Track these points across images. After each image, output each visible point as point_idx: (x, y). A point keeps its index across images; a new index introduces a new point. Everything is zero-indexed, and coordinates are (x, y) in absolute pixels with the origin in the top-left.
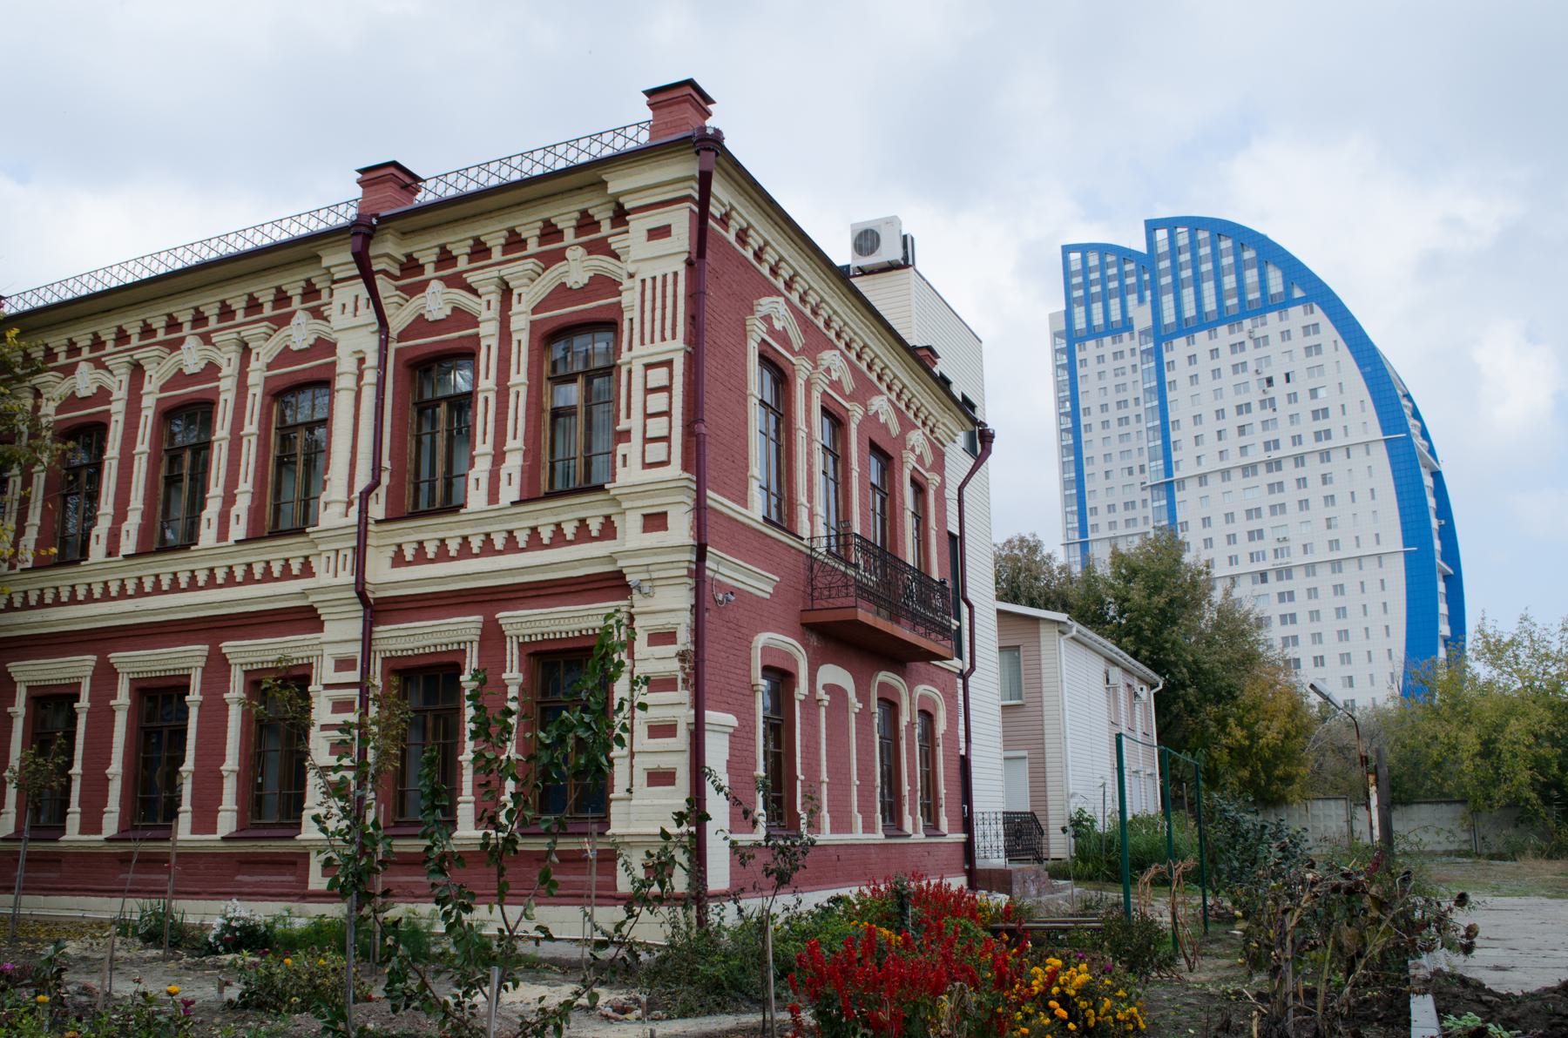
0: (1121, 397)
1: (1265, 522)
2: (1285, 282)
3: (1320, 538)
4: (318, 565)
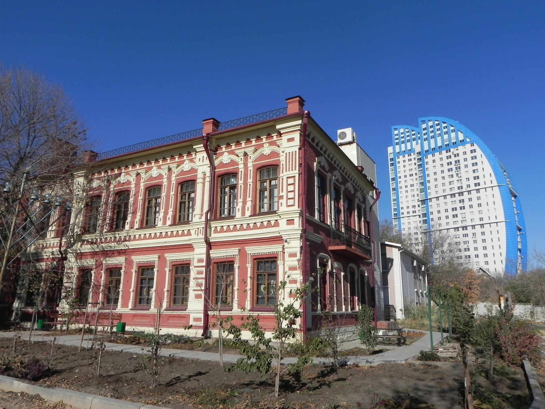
0: (411, 173)
1: (458, 212)
2: (464, 137)
3: (477, 217)
4: (192, 232)
